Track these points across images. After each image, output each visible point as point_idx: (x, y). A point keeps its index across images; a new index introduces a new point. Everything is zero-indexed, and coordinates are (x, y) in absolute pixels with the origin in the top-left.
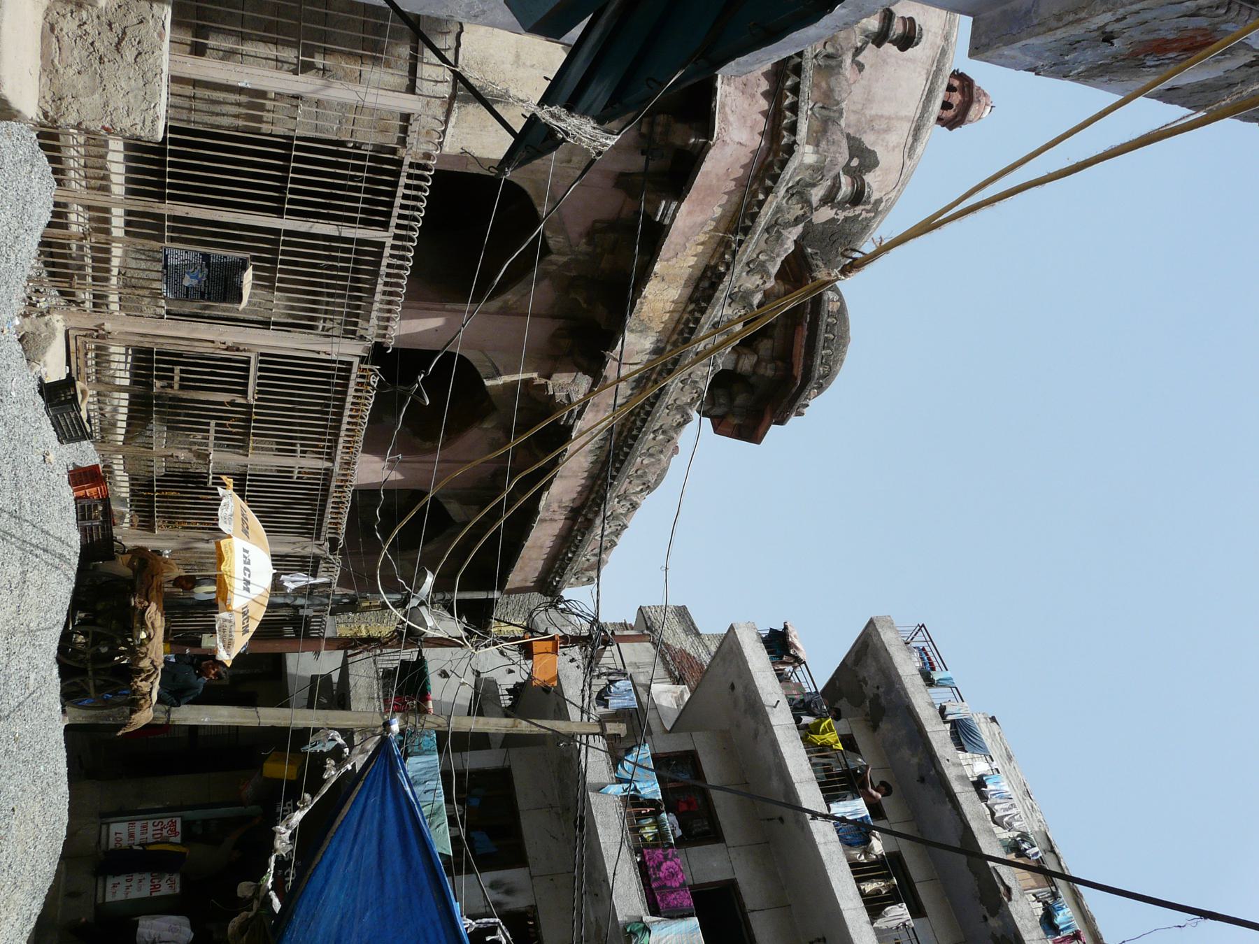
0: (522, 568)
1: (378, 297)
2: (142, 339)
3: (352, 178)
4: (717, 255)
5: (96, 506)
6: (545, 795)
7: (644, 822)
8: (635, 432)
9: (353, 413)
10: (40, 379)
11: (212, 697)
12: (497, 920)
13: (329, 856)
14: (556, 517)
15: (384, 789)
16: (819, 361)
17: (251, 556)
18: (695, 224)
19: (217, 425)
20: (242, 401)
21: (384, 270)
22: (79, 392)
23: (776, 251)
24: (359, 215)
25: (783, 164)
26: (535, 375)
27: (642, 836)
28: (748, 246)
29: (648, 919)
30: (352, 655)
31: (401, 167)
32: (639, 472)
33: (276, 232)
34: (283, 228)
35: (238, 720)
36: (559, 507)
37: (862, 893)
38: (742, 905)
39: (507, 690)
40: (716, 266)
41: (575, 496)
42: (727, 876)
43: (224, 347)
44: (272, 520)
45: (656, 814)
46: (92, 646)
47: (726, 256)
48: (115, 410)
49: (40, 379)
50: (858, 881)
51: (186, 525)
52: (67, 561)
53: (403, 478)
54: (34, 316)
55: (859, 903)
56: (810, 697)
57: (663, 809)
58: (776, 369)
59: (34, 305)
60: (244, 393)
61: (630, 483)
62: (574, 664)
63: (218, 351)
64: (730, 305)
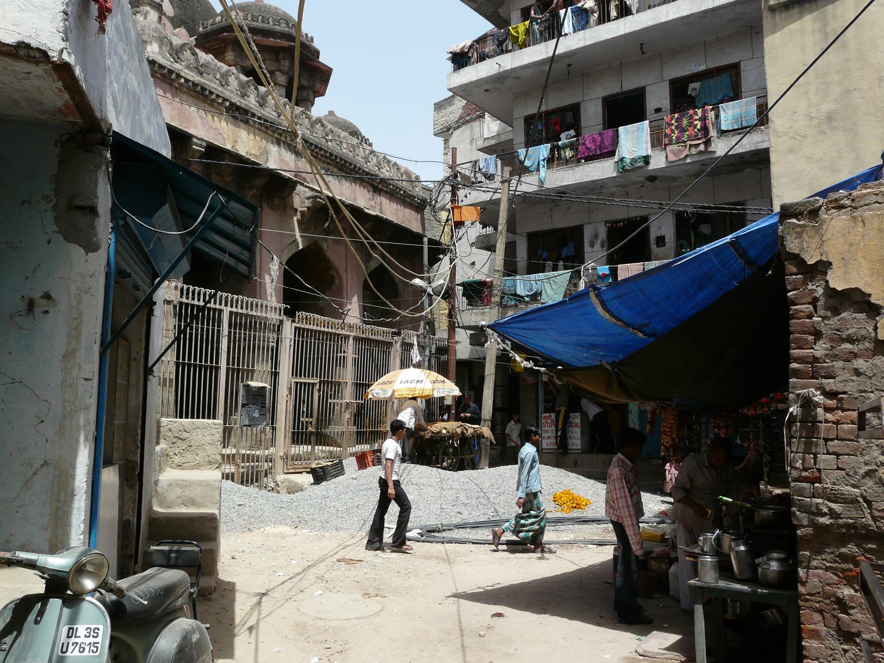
0: (410, 222)
1: (254, 313)
2: (287, 438)
3: (197, 330)
4: (219, 107)
5: (377, 456)
6: (544, 213)
7: (563, 156)
8: (328, 155)
9: (322, 326)
10: (311, 484)
11: (479, 400)
12: (583, 267)
13: (533, 346)
14: (379, 202)
15: (507, 327)
16: (278, 28)
17: (404, 380)
18: (202, 123)
19: (331, 398)
20: (318, 385)
21: (244, 311)
22: (318, 466)
23: (213, 67)
24: (252, 333)
25: (162, 67)
26: (295, 218)
27: (571, 158)
28: (213, 87)
29: (616, 158)
30: (458, 324)
31: (188, 304)
32: (352, 150)
33: (228, 369)
34: (225, 366)
35: (491, 386)
36: (373, 200)
37: (617, 18)
38: (618, 94)
39: (483, 228)
40: (226, 107)
41: (366, 190)
42: (600, 101)
43: (289, 395)
44: (381, 370)
45: (559, 148)
46: (449, 456)
47: (220, 101)
48: (322, 451)
49: (311, 484)
50: (609, 20)
51: (384, 414)
52: (406, 467)
53: (356, 296)
54: (278, 488)
55: (622, 21)
56: (495, 40)
57: (556, 143)
58: (284, 58)
59: (273, 488)
60: (313, 384)
61: (358, 155)
62: (468, 195)
63: (292, 399)
64: (248, 96)
